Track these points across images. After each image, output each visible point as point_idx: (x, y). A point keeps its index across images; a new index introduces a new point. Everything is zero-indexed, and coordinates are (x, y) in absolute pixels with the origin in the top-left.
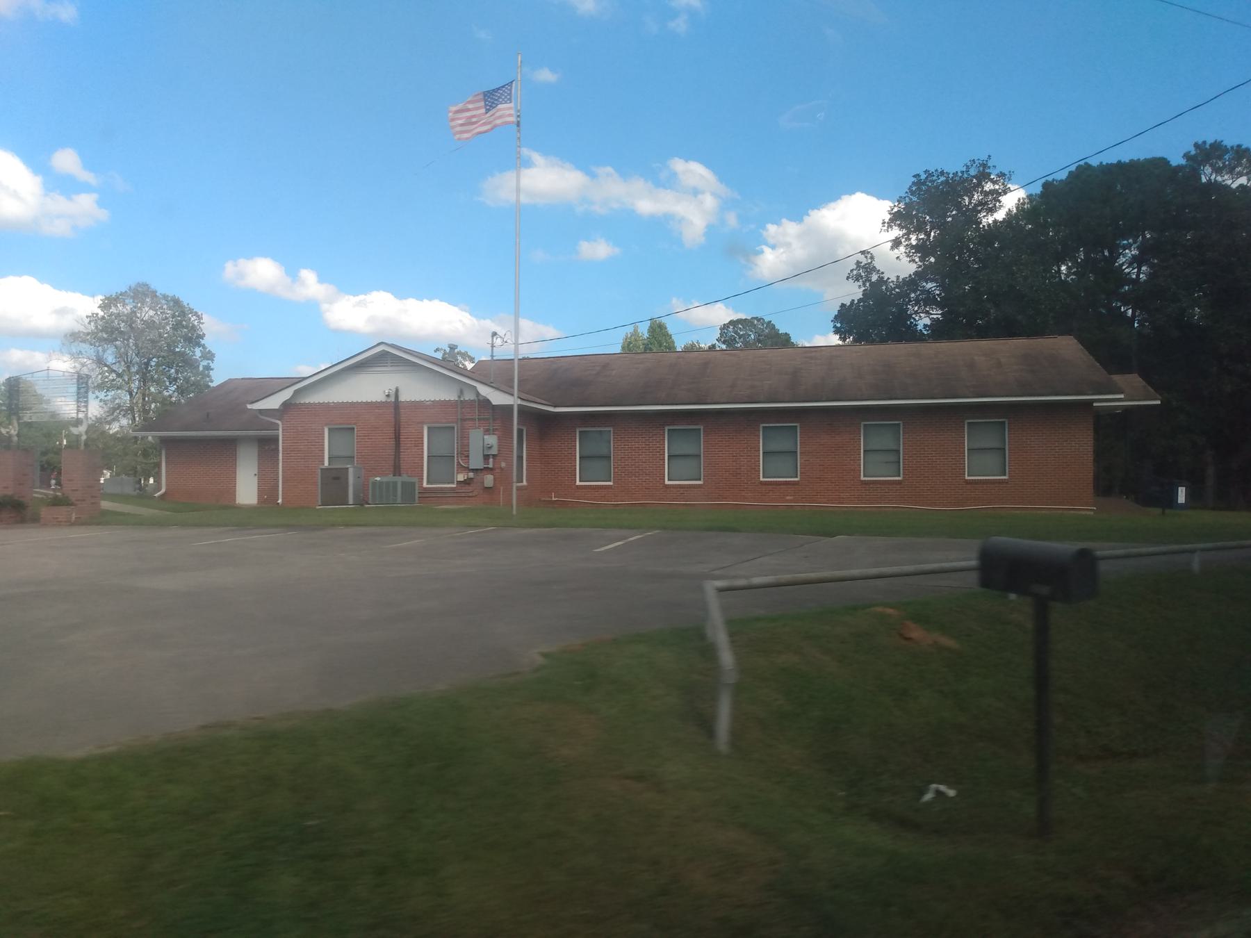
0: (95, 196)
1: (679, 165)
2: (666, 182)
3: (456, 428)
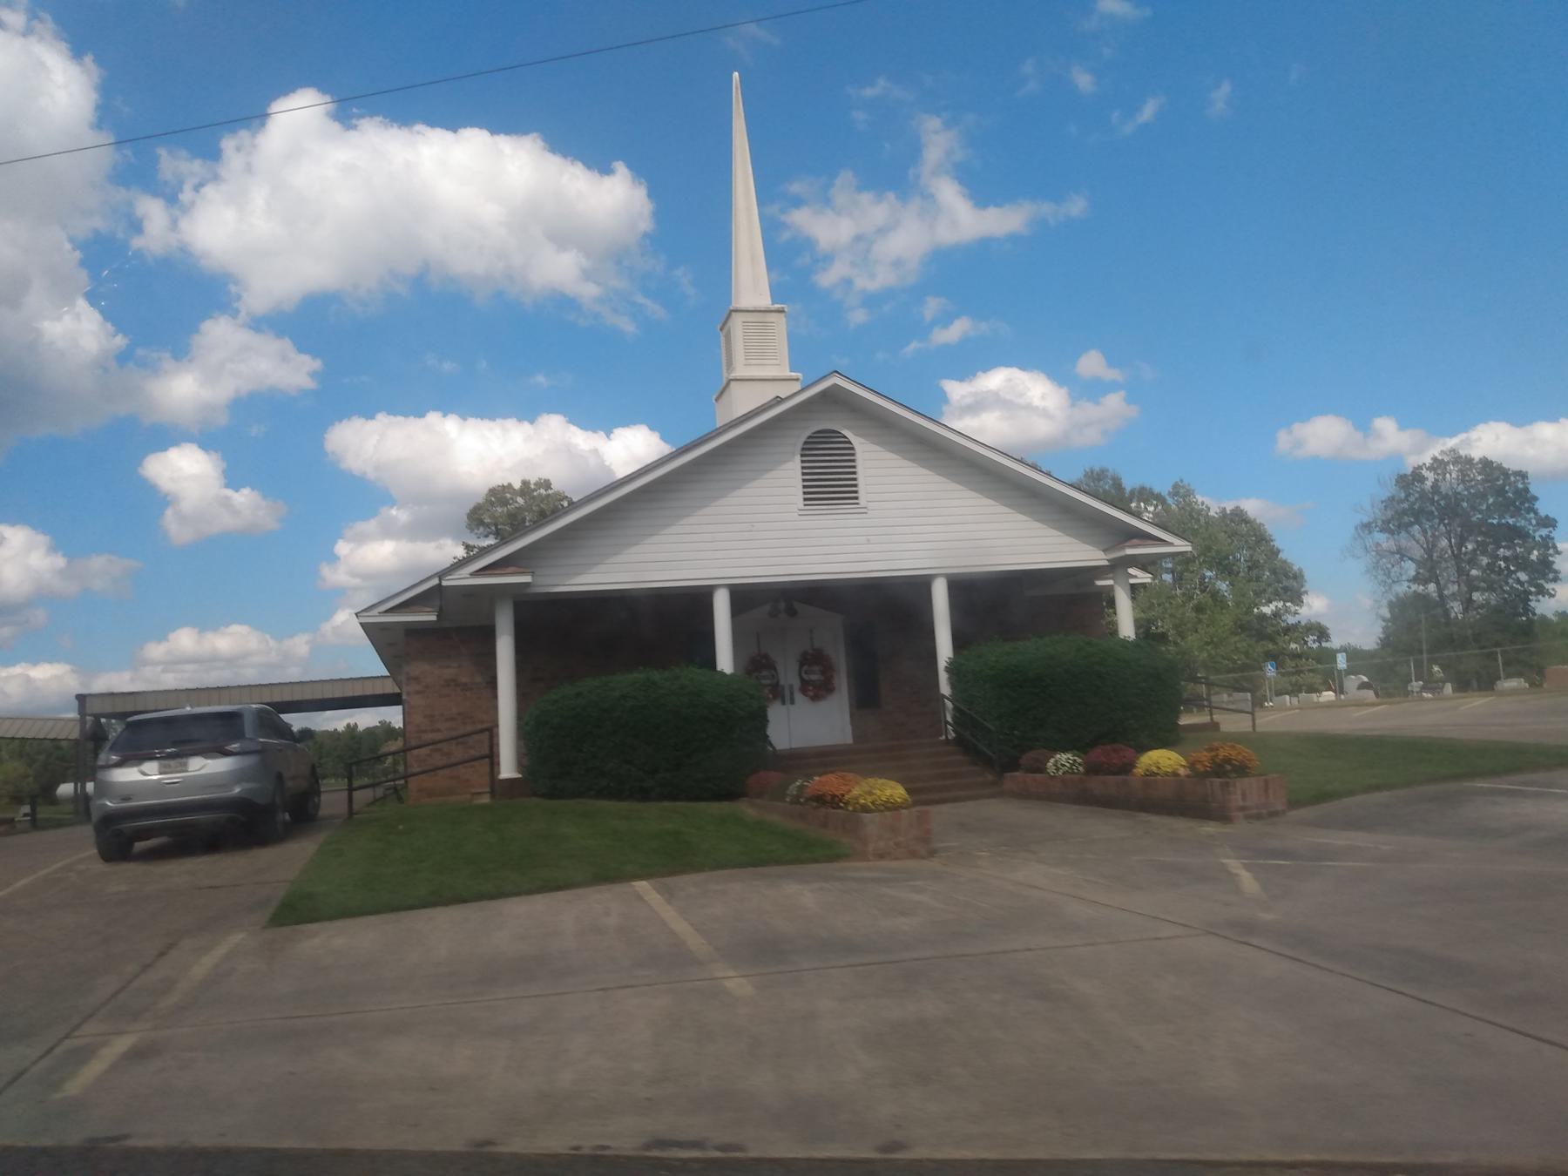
0: (1123, 393)
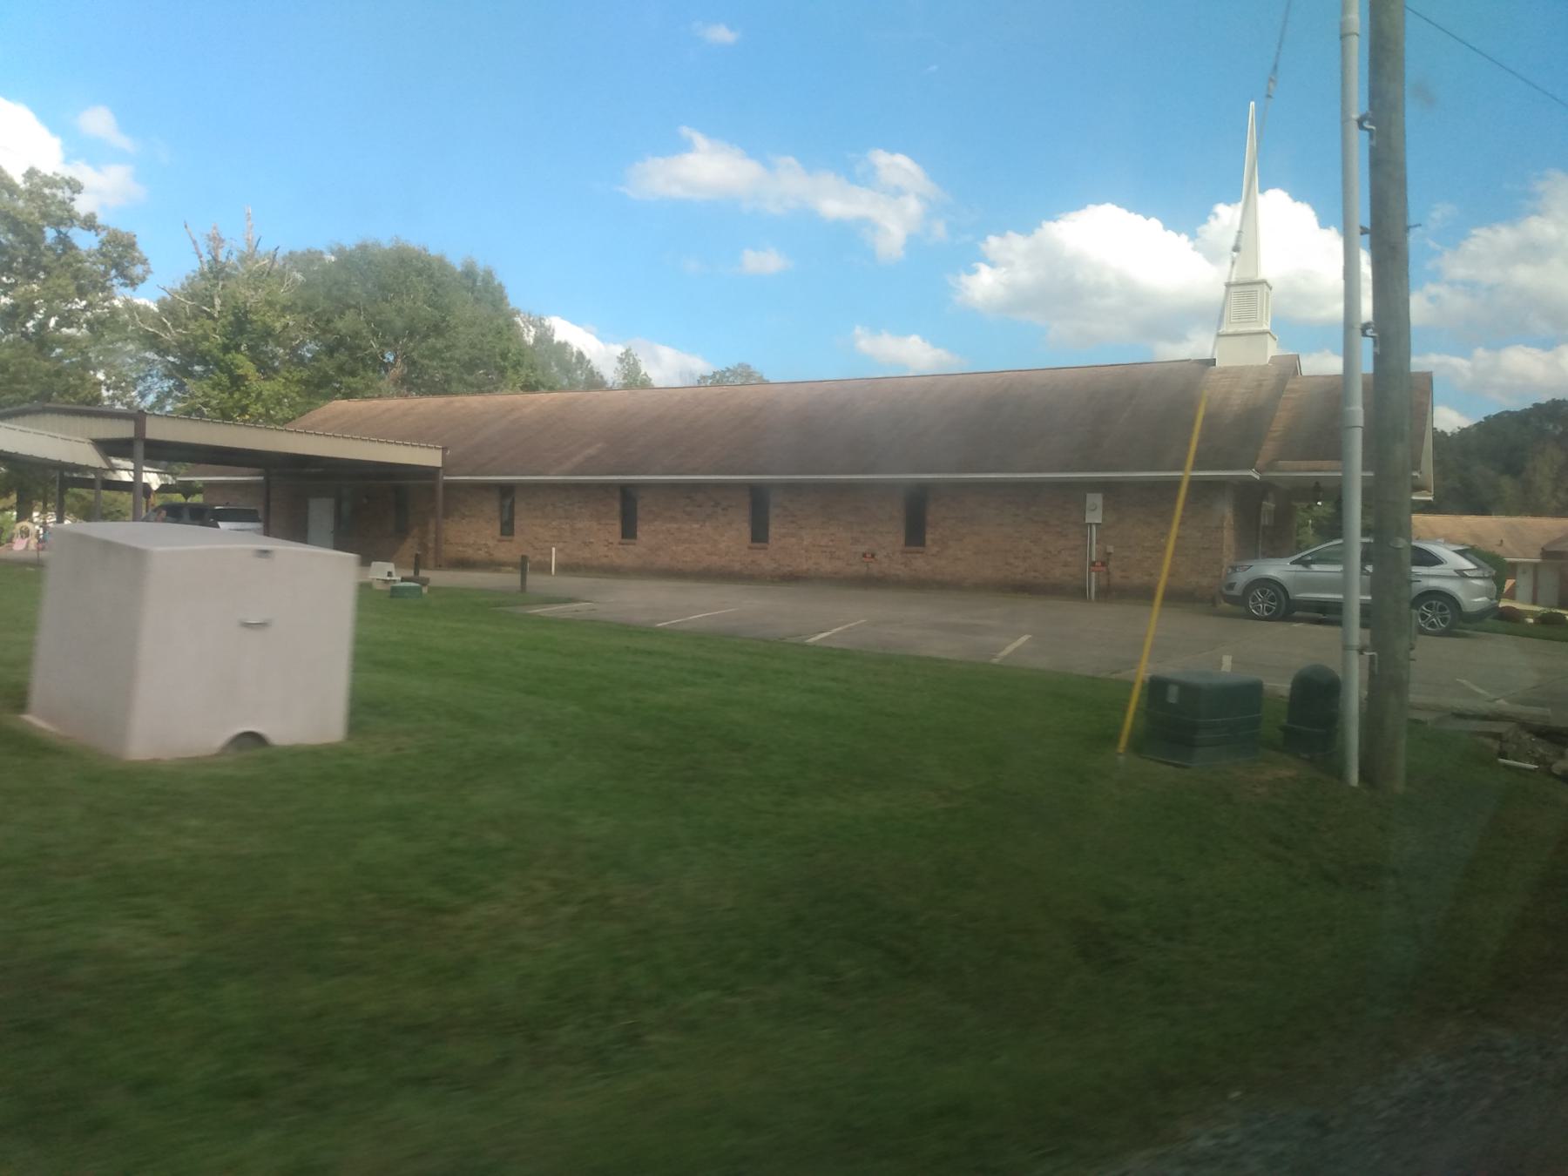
1: (882, 158)
2: (860, 177)
3: (1259, 293)
